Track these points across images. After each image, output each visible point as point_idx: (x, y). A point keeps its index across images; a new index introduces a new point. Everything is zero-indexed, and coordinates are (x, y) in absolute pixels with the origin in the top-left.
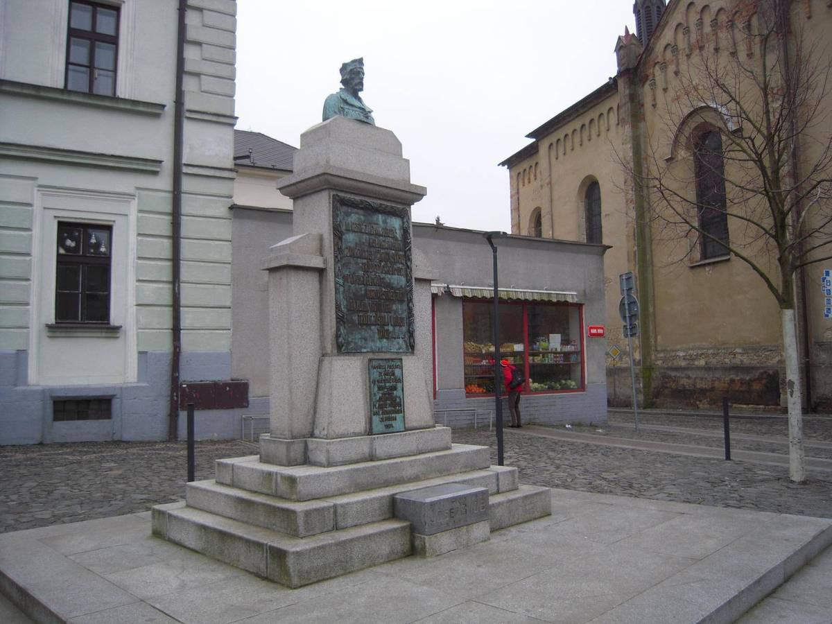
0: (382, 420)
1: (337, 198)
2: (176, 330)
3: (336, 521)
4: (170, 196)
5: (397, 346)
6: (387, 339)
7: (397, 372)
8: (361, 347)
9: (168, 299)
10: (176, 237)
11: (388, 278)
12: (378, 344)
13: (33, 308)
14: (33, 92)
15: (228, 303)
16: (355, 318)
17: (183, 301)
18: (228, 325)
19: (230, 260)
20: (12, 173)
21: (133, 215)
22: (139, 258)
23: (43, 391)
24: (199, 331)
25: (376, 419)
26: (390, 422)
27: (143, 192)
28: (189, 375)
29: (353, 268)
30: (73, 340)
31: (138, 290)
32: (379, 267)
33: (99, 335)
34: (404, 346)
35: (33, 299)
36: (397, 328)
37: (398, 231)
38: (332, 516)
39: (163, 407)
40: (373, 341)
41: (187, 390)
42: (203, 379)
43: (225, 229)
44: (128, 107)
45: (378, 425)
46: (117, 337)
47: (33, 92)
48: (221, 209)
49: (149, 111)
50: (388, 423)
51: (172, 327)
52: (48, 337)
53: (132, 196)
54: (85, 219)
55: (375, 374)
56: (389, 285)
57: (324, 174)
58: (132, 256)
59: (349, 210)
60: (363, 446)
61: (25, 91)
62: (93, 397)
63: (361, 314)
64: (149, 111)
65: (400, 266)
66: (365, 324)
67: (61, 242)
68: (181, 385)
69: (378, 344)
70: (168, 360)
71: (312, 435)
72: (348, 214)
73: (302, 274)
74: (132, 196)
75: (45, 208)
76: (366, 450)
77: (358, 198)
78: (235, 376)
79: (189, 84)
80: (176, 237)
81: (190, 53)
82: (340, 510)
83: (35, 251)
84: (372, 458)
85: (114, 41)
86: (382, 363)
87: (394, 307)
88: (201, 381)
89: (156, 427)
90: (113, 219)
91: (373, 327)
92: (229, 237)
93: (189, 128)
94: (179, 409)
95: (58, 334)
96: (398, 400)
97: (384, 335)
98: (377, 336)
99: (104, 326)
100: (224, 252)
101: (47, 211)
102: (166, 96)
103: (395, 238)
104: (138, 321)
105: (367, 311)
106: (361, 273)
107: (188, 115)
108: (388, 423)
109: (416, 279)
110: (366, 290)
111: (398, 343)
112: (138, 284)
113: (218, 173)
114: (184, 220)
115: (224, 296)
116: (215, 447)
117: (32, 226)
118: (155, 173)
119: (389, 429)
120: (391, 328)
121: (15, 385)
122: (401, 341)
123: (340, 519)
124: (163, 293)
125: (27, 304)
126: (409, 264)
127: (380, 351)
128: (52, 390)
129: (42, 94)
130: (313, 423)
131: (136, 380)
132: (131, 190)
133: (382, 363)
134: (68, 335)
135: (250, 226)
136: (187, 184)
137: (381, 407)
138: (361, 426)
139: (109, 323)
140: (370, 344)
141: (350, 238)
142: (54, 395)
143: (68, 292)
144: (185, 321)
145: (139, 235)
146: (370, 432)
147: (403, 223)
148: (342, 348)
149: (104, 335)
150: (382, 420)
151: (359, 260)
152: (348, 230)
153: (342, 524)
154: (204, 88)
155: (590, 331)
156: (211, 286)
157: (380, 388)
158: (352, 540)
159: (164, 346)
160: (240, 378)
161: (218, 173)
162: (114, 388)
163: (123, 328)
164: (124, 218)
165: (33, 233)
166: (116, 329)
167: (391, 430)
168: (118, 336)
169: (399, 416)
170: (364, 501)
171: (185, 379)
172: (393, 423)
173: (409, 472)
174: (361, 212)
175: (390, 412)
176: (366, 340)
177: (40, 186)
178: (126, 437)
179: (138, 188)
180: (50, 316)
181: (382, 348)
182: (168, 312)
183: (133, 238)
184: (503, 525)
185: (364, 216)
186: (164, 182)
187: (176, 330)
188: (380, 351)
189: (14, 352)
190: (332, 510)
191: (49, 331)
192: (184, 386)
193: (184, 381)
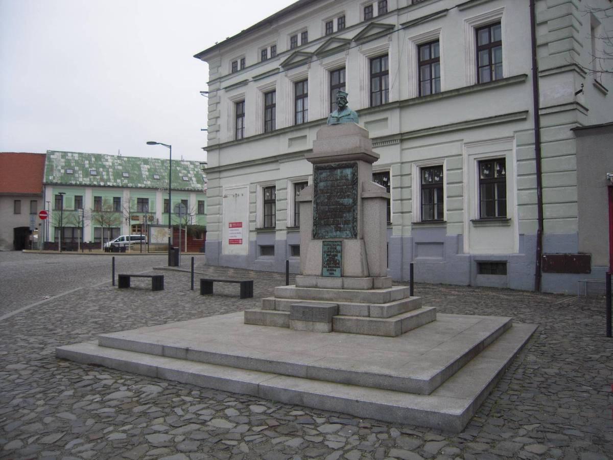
0: (328, 270)
2: (541, 219)
3: (275, 306)
5: (345, 235)
6: (340, 231)
7: (338, 248)
8: (325, 235)
9: (536, 200)
11: (341, 201)
12: (334, 234)
13: (465, 211)
14: (456, 93)
15: (575, 199)
16: (322, 222)
17: (544, 201)
19: (575, 168)
20: (409, 147)
21: (515, 149)
23: (470, 257)
25: (325, 269)
26: (333, 272)
27: (518, 133)
28: (548, 250)
29: (322, 199)
30: (487, 228)
31: (518, 195)
32: (337, 196)
33: (498, 224)
34: (350, 235)
35: (465, 206)
36: (346, 226)
37: (349, 176)
38: (274, 304)
39: (532, 270)
40: (332, 232)
41: (546, 259)
42: (558, 252)
43: (571, 147)
44: (468, 91)
45: (326, 273)
46: (510, 226)
47: (456, 93)
50: (331, 272)
51: (537, 217)
52: (475, 227)
53: (513, 137)
54: (486, 157)
55: (326, 249)
56: (342, 204)
58: (515, 174)
59: (322, 171)
60: (313, 281)
61: (454, 94)
62: (495, 261)
63: (325, 220)
65: (349, 193)
66: (327, 224)
67: (480, 172)
68: (543, 255)
69: (334, 234)
72: (321, 174)
74: (513, 137)
75: (469, 155)
77: (326, 164)
78: (581, 251)
82: (277, 303)
83: (465, 180)
86: (330, 243)
87: (345, 215)
88: (557, 253)
90: (503, 154)
91: (332, 226)
94: (542, 272)
95: (478, 225)
96: (338, 261)
97: (338, 229)
98: (334, 230)
99: (503, 219)
103: (347, 180)
104: (519, 214)
105: (328, 218)
106: (326, 200)
108: (331, 272)
110: (329, 208)
111: (346, 233)
112: (518, 192)
113: (563, 108)
117: (462, 166)
118: (525, 119)
119: (331, 275)
120: (342, 226)
121: (457, 253)
122: (348, 232)
123: (277, 306)
124: (533, 195)
125: (462, 209)
127: (335, 237)
128: (475, 257)
129: (461, 92)
130: (369, 272)
131: (518, 252)
133: (330, 243)
134: (483, 225)
137: (328, 264)
138: (319, 272)
139: (506, 217)
140: (330, 234)
141: (322, 184)
142: (477, 259)
143: (496, 198)
144: (546, 214)
145: (518, 161)
146: (322, 275)
149: (501, 224)
150: (328, 270)
151: (325, 195)
152: (321, 181)
153: (277, 309)
156: (563, 188)
157: (327, 255)
158: (266, 313)
160: (585, 252)
161: (563, 108)
162: (506, 256)
164: (510, 152)
165: (464, 170)
167: (333, 275)
169: (338, 270)
170: (287, 302)
171: (546, 252)
172: (334, 272)
173: (326, 296)
174: (328, 171)
175: (333, 267)
176: (328, 232)
177: (465, 144)
178: (512, 287)
180: (475, 215)
181: (337, 236)
184: (351, 331)
185: (330, 172)
186: (530, 124)
187: (541, 219)
188: (335, 237)
189: (456, 235)
190: (274, 302)
191: (473, 224)
192: (544, 256)
193: (546, 253)
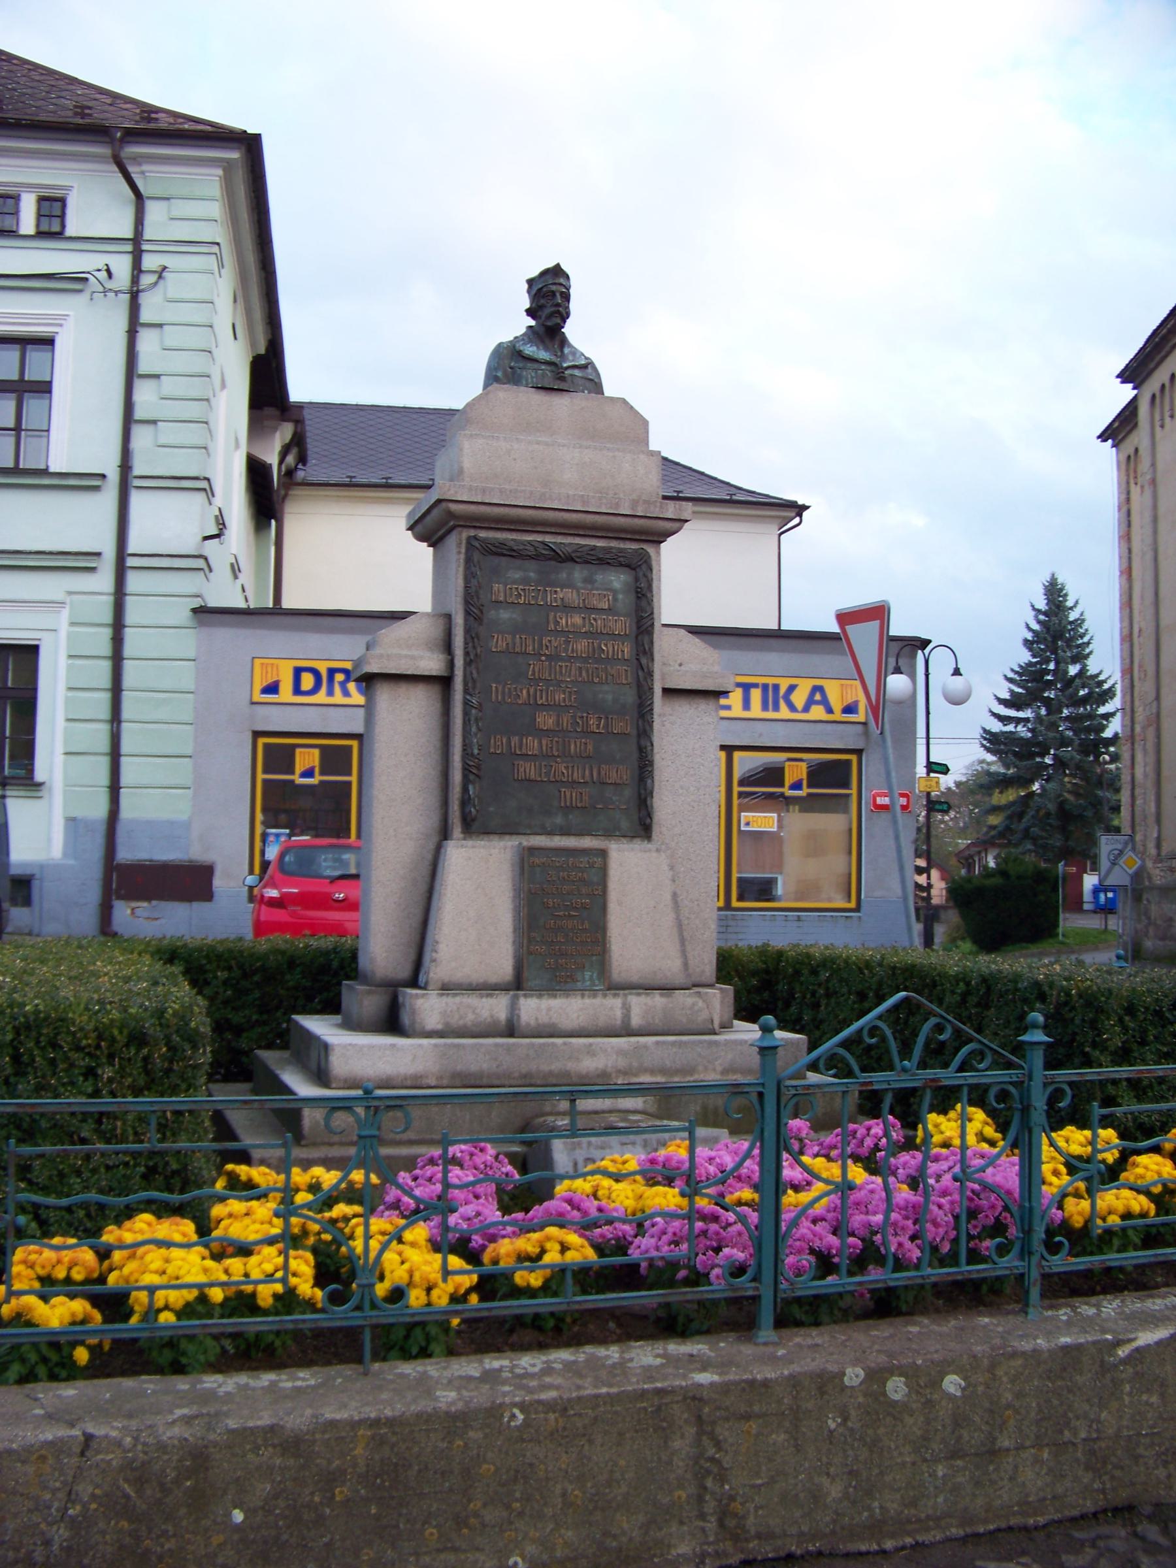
1: (476, 544)
4: (111, 599)
9: (104, 745)
10: (117, 658)
18: (189, 783)
21: (64, 628)
22: (70, 689)
24: (145, 791)
43: (188, 642)
48: (181, 613)
49: (88, 482)
57: (439, 501)
60: (496, 1007)
64: (88, 482)
70: (102, 829)
71: (414, 982)
73: (403, 689)
76: (502, 1015)
79: (141, 438)
80: (117, 658)
81: (144, 394)
84: (511, 1030)
85: (44, 388)
89: (85, 920)
92: (192, 655)
93: (137, 500)
100: (184, 674)
101: (207, 297)
102: (110, 466)
107: (137, 483)
109: (667, 692)
114: (129, 633)
115: (183, 739)
116: (809, 1341)
118: (92, 570)
126: (644, 661)
130: (418, 964)
132: (60, 596)
135: (225, 636)
136: (134, 582)
143: (8, 733)
145: (70, 657)
147: (637, 580)
148: (473, 826)
154: (162, 441)
155: (875, 800)
159: (99, 809)
163: (47, 785)
166: (40, 784)
168: (39, 794)
179: (70, 593)
182: (104, 763)
183: (63, 661)
186: (104, 580)
